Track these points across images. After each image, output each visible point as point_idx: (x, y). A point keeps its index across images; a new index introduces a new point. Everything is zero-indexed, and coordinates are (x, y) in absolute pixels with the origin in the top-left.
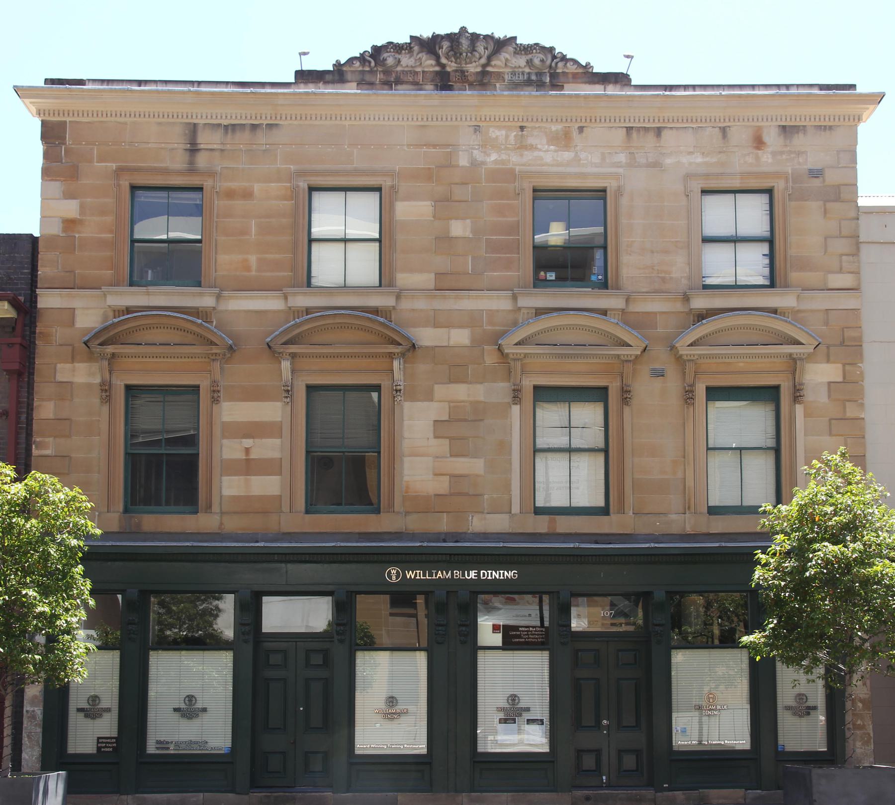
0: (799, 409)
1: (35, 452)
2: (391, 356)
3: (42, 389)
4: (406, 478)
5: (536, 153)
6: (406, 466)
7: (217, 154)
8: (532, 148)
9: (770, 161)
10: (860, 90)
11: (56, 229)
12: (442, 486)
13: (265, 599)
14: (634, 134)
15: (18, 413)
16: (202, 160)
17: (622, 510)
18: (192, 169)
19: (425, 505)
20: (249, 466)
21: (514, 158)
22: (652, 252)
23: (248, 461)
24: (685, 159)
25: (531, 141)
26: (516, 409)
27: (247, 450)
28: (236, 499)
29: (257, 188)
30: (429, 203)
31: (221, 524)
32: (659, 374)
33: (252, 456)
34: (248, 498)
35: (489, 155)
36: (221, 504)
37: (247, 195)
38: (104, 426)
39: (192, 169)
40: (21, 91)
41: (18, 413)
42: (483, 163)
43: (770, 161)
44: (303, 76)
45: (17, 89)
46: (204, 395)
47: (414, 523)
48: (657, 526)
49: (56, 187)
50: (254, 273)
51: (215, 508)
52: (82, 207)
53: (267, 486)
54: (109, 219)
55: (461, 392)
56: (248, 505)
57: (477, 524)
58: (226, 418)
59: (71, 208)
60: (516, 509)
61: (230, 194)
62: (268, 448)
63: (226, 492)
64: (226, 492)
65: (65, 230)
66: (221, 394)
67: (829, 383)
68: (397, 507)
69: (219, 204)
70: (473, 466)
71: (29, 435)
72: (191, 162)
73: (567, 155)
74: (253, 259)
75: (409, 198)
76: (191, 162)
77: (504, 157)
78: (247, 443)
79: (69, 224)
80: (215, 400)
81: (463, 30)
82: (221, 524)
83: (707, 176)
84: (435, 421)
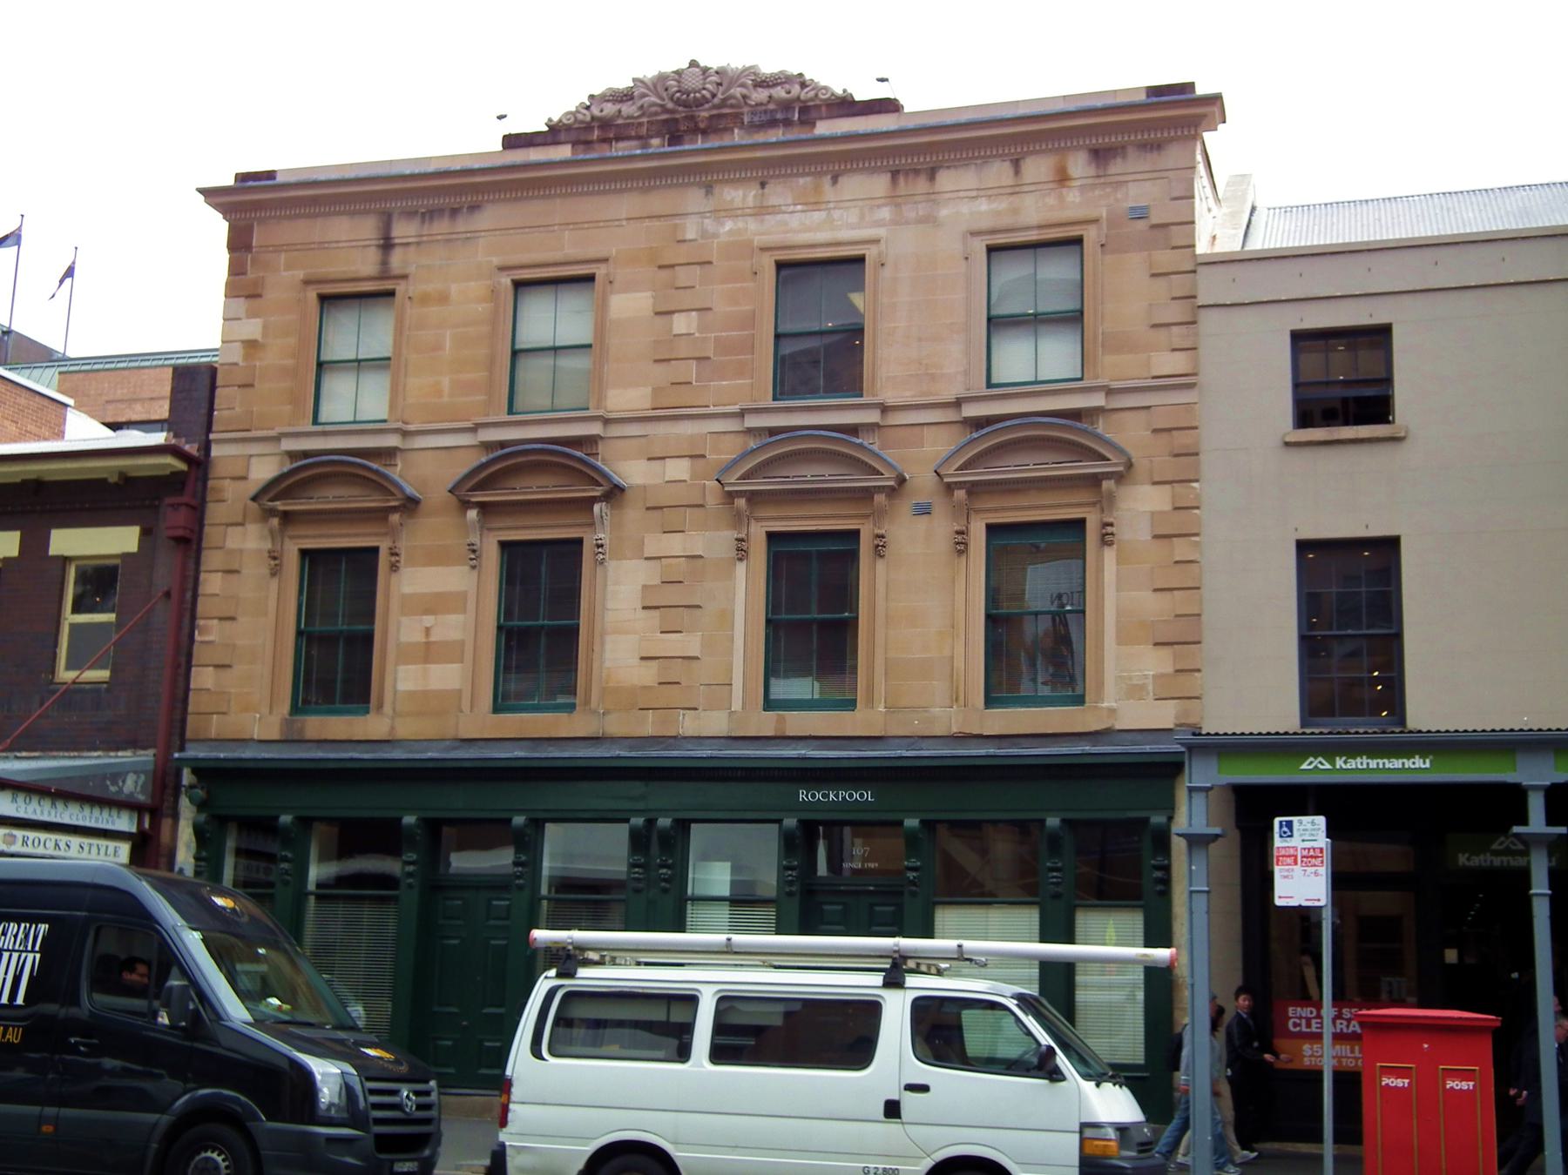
0: (1109, 555)
1: (197, 637)
2: (594, 500)
3: (211, 559)
4: (607, 664)
5: (779, 217)
6: (608, 647)
7: (412, 248)
8: (774, 210)
9: (1078, 200)
10: (1200, 90)
11: (236, 355)
12: (647, 675)
13: (693, 826)
14: (901, 180)
15: (183, 591)
16: (397, 259)
17: (870, 701)
18: (385, 275)
19: (636, 700)
20: (429, 652)
21: (752, 225)
22: (920, 340)
23: (428, 644)
24: (965, 208)
25: (774, 200)
26: (741, 568)
27: (428, 630)
28: (412, 695)
29: (454, 289)
30: (649, 294)
31: (393, 728)
32: (924, 510)
33: (432, 639)
34: (425, 693)
35: (723, 224)
36: (394, 703)
37: (443, 299)
38: (272, 604)
39: (385, 275)
40: (210, 194)
41: (183, 591)
42: (715, 235)
43: (1078, 200)
44: (511, 142)
45: (202, 191)
46: (383, 560)
47: (617, 725)
48: (914, 725)
49: (241, 305)
50: (446, 399)
51: (387, 708)
52: (265, 327)
53: (445, 677)
54: (292, 341)
55: (675, 545)
56: (427, 703)
57: (689, 725)
58: (407, 589)
59: (252, 329)
60: (737, 705)
61: (425, 300)
62: (451, 627)
63: (403, 686)
64: (403, 686)
65: (247, 357)
66: (402, 558)
67: (1153, 513)
68: (594, 704)
69: (412, 312)
70: (688, 643)
71: (193, 618)
72: (385, 263)
73: (818, 216)
74: (446, 382)
75: (629, 287)
76: (385, 263)
77: (741, 225)
78: (429, 620)
79: (251, 345)
80: (394, 567)
81: (801, 75)
82: (393, 728)
83: (993, 232)
84: (644, 587)
